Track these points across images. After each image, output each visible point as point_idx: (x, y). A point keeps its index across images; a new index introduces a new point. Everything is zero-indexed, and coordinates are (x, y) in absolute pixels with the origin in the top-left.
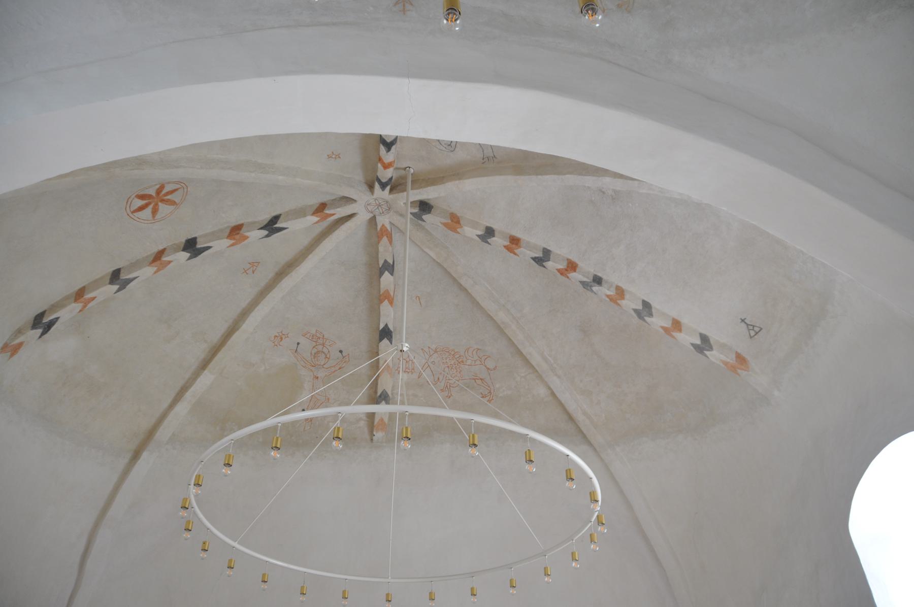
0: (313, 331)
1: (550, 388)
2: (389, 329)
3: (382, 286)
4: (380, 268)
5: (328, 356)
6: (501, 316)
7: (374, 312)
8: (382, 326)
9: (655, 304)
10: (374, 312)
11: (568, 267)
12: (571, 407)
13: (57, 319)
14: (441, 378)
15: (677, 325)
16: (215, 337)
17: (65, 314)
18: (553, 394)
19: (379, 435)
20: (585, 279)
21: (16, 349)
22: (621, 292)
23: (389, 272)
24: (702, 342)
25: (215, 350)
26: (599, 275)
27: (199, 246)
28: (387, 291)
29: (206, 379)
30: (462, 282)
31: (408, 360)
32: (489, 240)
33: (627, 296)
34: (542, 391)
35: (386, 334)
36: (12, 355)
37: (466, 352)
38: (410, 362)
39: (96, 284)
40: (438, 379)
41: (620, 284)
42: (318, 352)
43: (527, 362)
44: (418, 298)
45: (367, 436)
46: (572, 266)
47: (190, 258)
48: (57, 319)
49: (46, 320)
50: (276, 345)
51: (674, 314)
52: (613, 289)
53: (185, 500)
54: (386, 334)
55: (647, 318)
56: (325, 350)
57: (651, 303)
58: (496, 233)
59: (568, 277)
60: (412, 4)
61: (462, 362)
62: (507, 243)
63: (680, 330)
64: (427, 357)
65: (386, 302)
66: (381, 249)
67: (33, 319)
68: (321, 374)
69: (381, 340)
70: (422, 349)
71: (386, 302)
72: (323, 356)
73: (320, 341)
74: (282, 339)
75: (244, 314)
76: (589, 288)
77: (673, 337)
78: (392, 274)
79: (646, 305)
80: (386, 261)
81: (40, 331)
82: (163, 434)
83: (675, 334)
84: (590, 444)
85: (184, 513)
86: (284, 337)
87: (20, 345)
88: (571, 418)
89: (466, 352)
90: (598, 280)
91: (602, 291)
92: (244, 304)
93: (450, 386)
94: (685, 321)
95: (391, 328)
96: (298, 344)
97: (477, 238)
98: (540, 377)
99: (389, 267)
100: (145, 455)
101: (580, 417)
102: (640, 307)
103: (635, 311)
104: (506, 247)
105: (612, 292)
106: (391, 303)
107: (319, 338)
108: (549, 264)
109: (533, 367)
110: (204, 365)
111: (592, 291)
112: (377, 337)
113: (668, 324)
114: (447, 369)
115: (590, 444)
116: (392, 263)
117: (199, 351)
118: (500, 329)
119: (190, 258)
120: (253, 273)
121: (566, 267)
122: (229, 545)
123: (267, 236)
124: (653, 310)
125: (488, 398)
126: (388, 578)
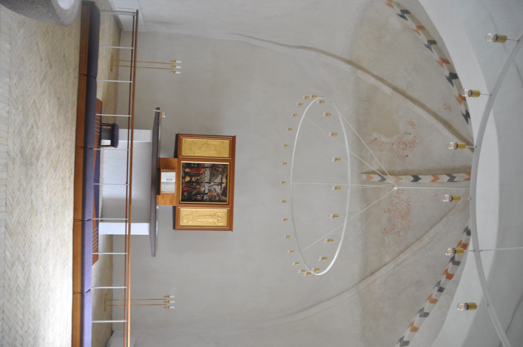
0: (417, 141)
1: (388, 263)
2: (419, 180)
3: (441, 176)
4: (451, 175)
5: (404, 150)
6: (426, 239)
7: (428, 172)
8: (420, 176)
9: (427, 319)
10: (428, 172)
11: (449, 274)
12: (378, 274)
13: (407, 20)
14: (395, 207)
15: (415, 329)
16: (410, 93)
17: (410, 23)
18: (385, 265)
19: (364, 177)
20: (442, 283)
21: (390, 5)
22: (434, 301)
23: (450, 179)
24: (404, 341)
25: (403, 93)
26: (445, 291)
27: (453, 81)
28: (438, 179)
29: (388, 90)
30: (445, 219)
31: (404, 190)
32: (465, 232)
33: (431, 305)
34: (387, 259)
35: (416, 179)
36: (387, 4)
37: (408, 221)
38: (402, 192)
39: (427, 34)
40: (394, 206)
41: (438, 302)
42: (406, 144)
43: (402, 252)
44: (436, 195)
45: (364, 171)
46: (449, 277)
47: (446, 77)
48: (407, 20)
49: (406, 15)
50: (408, 123)
51: (421, 329)
52: (436, 298)
53: (316, 96)
54: (416, 179)
55: (419, 314)
56: (407, 148)
57: (428, 317)
58: (468, 236)
59: (443, 274)
60: (55, 171)
61: (403, 219)
62: (463, 242)
63: (411, 331)
64: (406, 200)
65: (433, 178)
66: (462, 175)
67: (406, 9)
68: (395, 147)
69: (413, 176)
70: (409, 198)
71: (433, 178)
72: (404, 147)
73: (412, 145)
74: (412, 125)
75: (422, 106)
76: (437, 285)
77: (408, 327)
78: (448, 181)
79: (426, 315)
80: (455, 177)
81: (400, 13)
82: (360, 73)
83: (410, 329)
84: (360, 282)
85: (311, 96)
86: (413, 126)
87: (392, 7)
88: (373, 273)
89: (408, 221)
90: (441, 290)
91: (435, 292)
92: (428, 105)
93: (390, 212)
94: (417, 334)
95: (420, 181)
96: (410, 134)
97: (466, 226)
98: (394, 258)
99: (452, 179)
100: (350, 67)
101: (372, 278)
102: (425, 311)
103: (423, 309)
104: (461, 242)
105: (434, 297)
106: (433, 181)
107: (414, 144)
108: (451, 264)
109: (399, 255)
110: (395, 89)
111: (435, 287)
112: (415, 174)
113: (415, 325)
114: (399, 210)
115: (360, 282)
116: (454, 180)
117: (401, 84)
118: (419, 239)
119: (446, 77)
120: (445, 108)
121: (449, 273)
122: (303, 113)
123: (463, 114)
124: (423, 318)
125: (384, 231)
126: (292, 182)
